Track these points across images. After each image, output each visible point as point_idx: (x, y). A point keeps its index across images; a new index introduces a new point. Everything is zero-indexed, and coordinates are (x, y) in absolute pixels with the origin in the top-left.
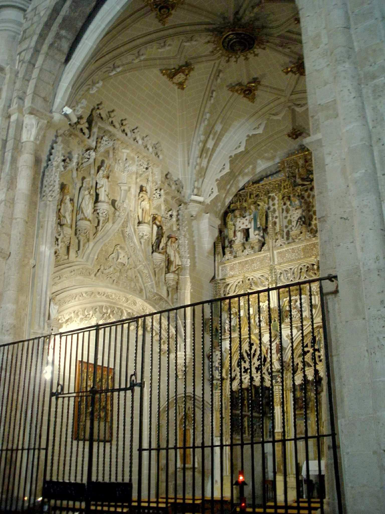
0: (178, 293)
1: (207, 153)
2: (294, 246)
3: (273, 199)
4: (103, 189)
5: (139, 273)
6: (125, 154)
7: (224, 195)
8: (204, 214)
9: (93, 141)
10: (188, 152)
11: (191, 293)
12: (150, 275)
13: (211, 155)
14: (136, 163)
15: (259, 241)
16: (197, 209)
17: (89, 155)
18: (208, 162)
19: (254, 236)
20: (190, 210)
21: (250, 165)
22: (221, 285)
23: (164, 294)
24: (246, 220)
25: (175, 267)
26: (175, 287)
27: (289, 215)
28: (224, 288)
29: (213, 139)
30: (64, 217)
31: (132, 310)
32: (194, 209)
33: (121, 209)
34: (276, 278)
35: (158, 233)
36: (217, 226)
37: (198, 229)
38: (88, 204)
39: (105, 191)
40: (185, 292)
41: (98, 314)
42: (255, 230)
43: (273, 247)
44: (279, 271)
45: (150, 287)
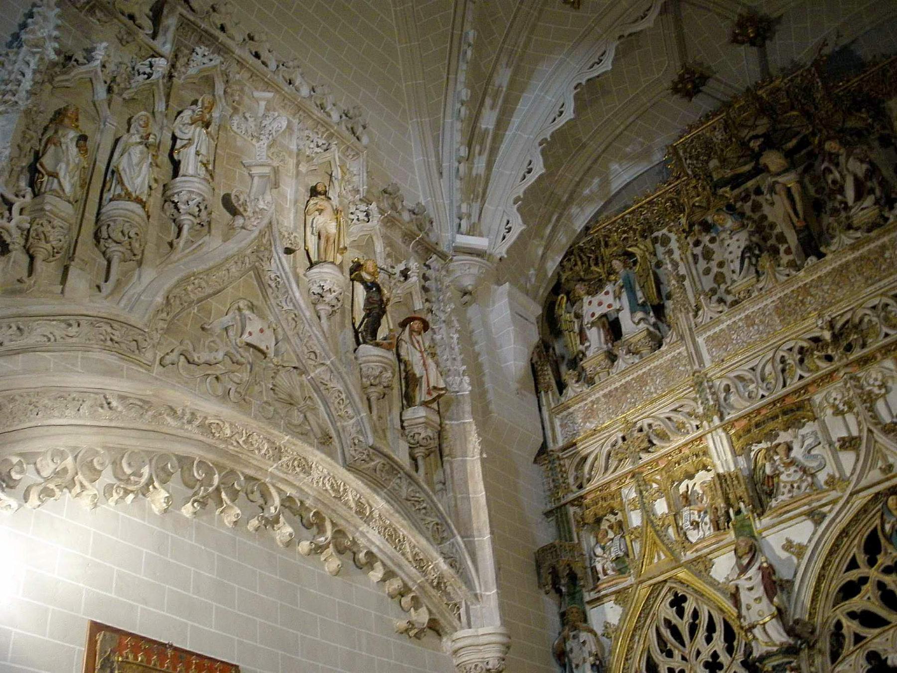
0: (447, 466)
1: (482, 143)
3: (665, 241)
4: (192, 150)
5: (317, 390)
6: (263, 104)
7: (540, 252)
9: (164, 44)
10: (436, 147)
11: (483, 461)
12: (349, 395)
13: (494, 151)
14: (296, 134)
15: (650, 333)
16: (475, 270)
17: (151, 66)
18: (490, 165)
19: (633, 327)
20: (458, 273)
21: (593, 178)
22: (567, 462)
23: (404, 459)
24: (607, 293)
25: (429, 393)
26: (434, 444)
27: (713, 264)
28: (576, 470)
29: (493, 107)
30: (54, 175)
31: (301, 490)
32: (466, 272)
33: (249, 213)
34: (717, 400)
35: (368, 301)
36: (533, 319)
37: (485, 324)
38: (139, 164)
39: (198, 153)
40: (464, 462)
41: (175, 482)
42: (633, 312)
43: (690, 329)
44: (720, 384)
45: (353, 430)
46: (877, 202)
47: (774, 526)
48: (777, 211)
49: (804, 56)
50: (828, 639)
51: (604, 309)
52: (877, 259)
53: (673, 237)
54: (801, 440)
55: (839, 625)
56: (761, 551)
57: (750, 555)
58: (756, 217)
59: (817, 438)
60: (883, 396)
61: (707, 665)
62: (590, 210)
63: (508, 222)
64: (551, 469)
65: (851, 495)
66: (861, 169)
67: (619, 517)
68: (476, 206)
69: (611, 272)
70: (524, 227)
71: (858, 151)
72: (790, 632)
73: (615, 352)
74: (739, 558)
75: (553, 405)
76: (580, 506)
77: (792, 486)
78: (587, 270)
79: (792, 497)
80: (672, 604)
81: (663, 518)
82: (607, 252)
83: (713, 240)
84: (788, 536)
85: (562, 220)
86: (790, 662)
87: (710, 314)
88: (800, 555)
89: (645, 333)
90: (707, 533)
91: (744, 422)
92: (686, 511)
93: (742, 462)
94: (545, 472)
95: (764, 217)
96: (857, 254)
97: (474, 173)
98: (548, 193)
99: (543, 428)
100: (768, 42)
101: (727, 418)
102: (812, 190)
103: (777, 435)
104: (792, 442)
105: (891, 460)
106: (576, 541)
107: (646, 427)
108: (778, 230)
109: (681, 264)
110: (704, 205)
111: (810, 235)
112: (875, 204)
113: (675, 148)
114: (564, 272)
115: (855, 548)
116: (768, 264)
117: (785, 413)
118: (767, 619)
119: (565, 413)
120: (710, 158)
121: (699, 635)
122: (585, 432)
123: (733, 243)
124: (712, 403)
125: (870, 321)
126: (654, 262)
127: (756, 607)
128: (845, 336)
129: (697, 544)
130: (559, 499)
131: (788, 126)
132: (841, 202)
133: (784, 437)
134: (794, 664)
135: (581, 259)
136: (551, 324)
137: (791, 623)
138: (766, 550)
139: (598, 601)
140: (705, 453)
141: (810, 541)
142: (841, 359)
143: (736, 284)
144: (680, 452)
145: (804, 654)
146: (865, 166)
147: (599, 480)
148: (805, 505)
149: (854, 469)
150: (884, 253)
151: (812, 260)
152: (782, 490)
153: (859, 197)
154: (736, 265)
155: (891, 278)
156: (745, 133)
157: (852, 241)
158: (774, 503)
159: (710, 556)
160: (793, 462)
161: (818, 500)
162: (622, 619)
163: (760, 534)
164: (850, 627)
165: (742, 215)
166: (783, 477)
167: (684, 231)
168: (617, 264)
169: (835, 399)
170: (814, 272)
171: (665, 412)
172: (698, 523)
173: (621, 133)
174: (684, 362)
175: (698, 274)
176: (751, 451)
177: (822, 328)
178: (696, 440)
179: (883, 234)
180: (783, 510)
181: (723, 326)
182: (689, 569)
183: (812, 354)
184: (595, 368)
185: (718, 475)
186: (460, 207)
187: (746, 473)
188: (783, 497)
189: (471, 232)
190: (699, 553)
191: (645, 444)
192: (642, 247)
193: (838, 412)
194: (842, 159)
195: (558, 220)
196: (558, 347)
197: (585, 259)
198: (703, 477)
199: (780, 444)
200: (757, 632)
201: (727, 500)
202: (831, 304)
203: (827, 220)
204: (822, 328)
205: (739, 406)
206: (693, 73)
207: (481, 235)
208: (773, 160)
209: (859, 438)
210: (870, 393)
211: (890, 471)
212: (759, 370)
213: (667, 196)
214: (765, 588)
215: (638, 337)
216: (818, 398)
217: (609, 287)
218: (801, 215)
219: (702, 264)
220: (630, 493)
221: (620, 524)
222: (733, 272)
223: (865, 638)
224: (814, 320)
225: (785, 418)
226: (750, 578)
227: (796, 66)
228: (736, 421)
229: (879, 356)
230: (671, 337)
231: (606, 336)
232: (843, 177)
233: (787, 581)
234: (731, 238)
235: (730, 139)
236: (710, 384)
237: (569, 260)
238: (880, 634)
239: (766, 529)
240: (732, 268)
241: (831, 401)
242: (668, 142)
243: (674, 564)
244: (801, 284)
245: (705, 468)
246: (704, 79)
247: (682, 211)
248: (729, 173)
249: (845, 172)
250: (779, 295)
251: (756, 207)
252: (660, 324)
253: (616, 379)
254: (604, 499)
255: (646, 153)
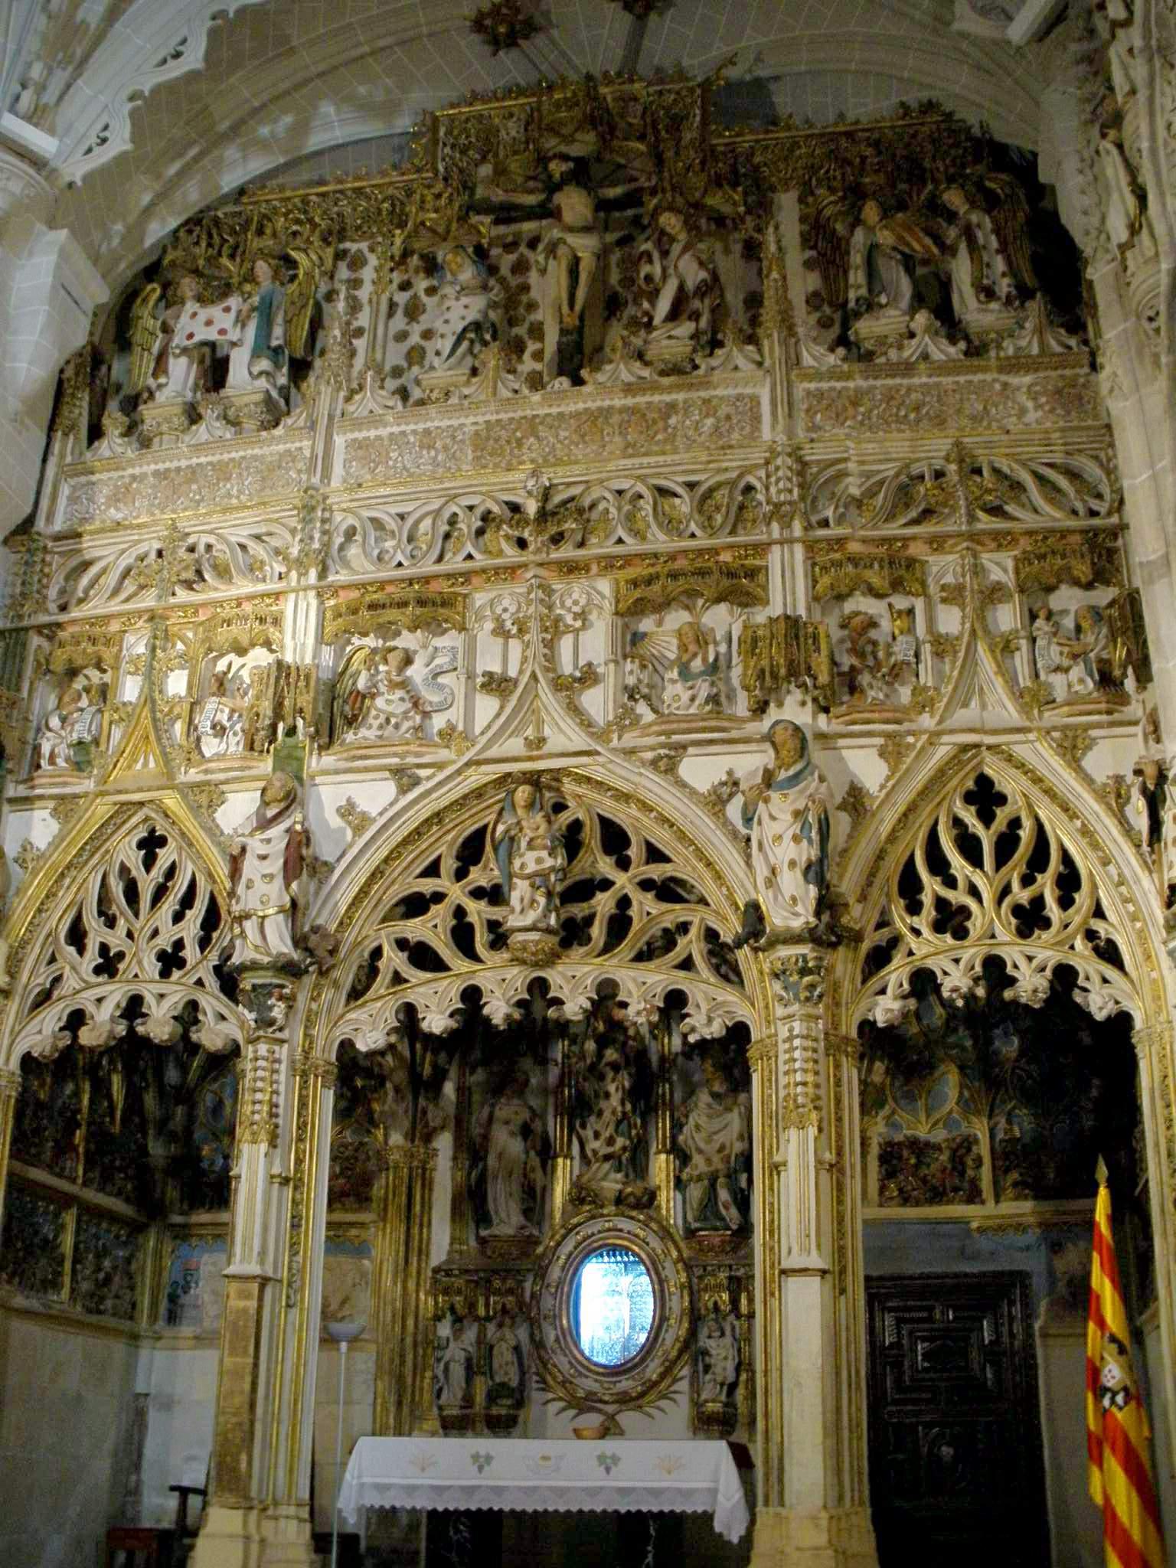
2: (435, 420)
7: (146, 199)
8: (40, 227)
15: (268, 400)
16: (16, 186)
19: (247, 378)
21: (285, 113)
24: (227, 310)
28: (67, 579)
34: (326, 545)
36: (89, 306)
42: (256, 354)
43: (331, 417)
44: (342, 521)
46: (695, 336)
47: (337, 772)
48: (548, 288)
49: (698, 65)
50: (355, 968)
51: (212, 335)
52: (655, 422)
53: (373, 260)
54: (432, 653)
55: (377, 953)
56: (302, 805)
57: (283, 805)
58: (514, 282)
59: (454, 659)
60: (577, 631)
61: (162, 956)
62: (258, 165)
63: (106, 128)
64: (26, 563)
65: (468, 764)
66: (694, 275)
67: (107, 678)
68: (60, 77)
69: (250, 278)
70: (129, 147)
71: (701, 246)
72: (299, 941)
73: (202, 410)
74: (265, 804)
75: (69, 459)
76: (50, 639)
77: (388, 721)
78: (212, 261)
79: (380, 737)
80: (141, 845)
81: (172, 703)
82: (255, 243)
83: (431, 291)
84: (355, 797)
85: (206, 161)
86: (282, 987)
87: (372, 405)
88: (358, 830)
89: (259, 397)
90: (232, 749)
91: (355, 594)
92: (211, 704)
93: (328, 655)
94: (15, 564)
95: (525, 288)
96: (630, 401)
97: (80, 15)
98: (198, 107)
99: (38, 493)
100: (653, 17)
101: (331, 578)
102: (614, 277)
103: (398, 634)
104: (415, 652)
105: (547, 731)
106: (25, 694)
107: (201, 548)
108: (537, 316)
109: (367, 309)
110: (441, 230)
111: (579, 346)
112: (692, 338)
113: (435, 120)
114: (175, 248)
115: (445, 846)
116: (493, 363)
117: (421, 602)
118: (271, 911)
119: (83, 479)
120: (484, 159)
121: (165, 907)
122: (103, 521)
123: (457, 307)
124: (316, 545)
125: (607, 511)
126: (323, 288)
127: (260, 887)
128: (557, 518)
129: (210, 761)
130: (20, 617)
131: (623, 161)
132: (646, 313)
133: (407, 640)
134: (286, 991)
135: (210, 236)
136: (119, 325)
137: (306, 929)
138: (311, 807)
139: (25, 802)
140: (277, 622)
141: (381, 814)
142: (538, 551)
143: (433, 374)
144: (239, 605)
145: (309, 980)
146: (703, 275)
147: (94, 607)
148: (395, 755)
149: (489, 727)
150: (669, 417)
151: (564, 382)
152: (371, 720)
153: (674, 315)
154: (446, 345)
155: (661, 459)
156: (551, 143)
157: (632, 379)
158: (350, 737)
159: (224, 787)
160: (404, 685)
161: (418, 755)
162: (55, 844)
163: (312, 778)
164: (393, 959)
165: (493, 270)
166: (380, 702)
167: (392, 257)
168: (262, 269)
169: (505, 610)
170: (567, 401)
171: (241, 535)
172: (223, 729)
173: (362, 57)
174: (300, 465)
175: (386, 335)
176: (349, 642)
177: (530, 493)
178: (269, 595)
179: (678, 388)
180: (363, 751)
181: (384, 432)
182: (185, 797)
183: (499, 528)
184: (159, 424)
185: (279, 664)
186: (29, 65)
187: (326, 675)
188: (367, 733)
189: (35, 117)
190: (209, 777)
191: (190, 575)
192: (314, 257)
193: (500, 631)
194: (676, 249)
195: (196, 159)
196: (118, 368)
197: (216, 240)
198: (260, 657)
199: (395, 648)
200: (250, 926)
201: (278, 707)
202: (559, 462)
203: (616, 332)
204: (530, 493)
205: (358, 566)
206: (518, 11)
207: (51, 131)
208: (574, 204)
209: (516, 682)
210: (558, 619)
211: (539, 748)
212: (410, 521)
213: (390, 191)
214: (286, 863)
215: (246, 399)
216: (480, 599)
217: (234, 301)
218: (578, 307)
219: (399, 322)
220: (137, 645)
221: (104, 692)
222: (438, 353)
223: (406, 981)
224: (522, 476)
225: (419, 611)
226: (268, 841)
227: (681, 75)
228: (343, 587)
229: (594, 568)
230: (297, 418)
231: (197, 379)
232: (665, 276)
233: (326, 863)
234: (457, 299)
235: (527, 143)
236: (327, 515)
237: (190, 232)
238: (429, 981)
239: (325, 772)
240: (439, 346)
241: (499, 610)
242: (429, 107)
243: (163, 781)
244: (529, 413)
245: (268, 644)
246: (530, 28)
247: (402, 225)
248: (499, 196)
249: (671, 271)
250: (488, 417)
251: (521, 267)
252: (293, 391)
253: (179, 453)
254: (93, 641)
255: (389, 109)
